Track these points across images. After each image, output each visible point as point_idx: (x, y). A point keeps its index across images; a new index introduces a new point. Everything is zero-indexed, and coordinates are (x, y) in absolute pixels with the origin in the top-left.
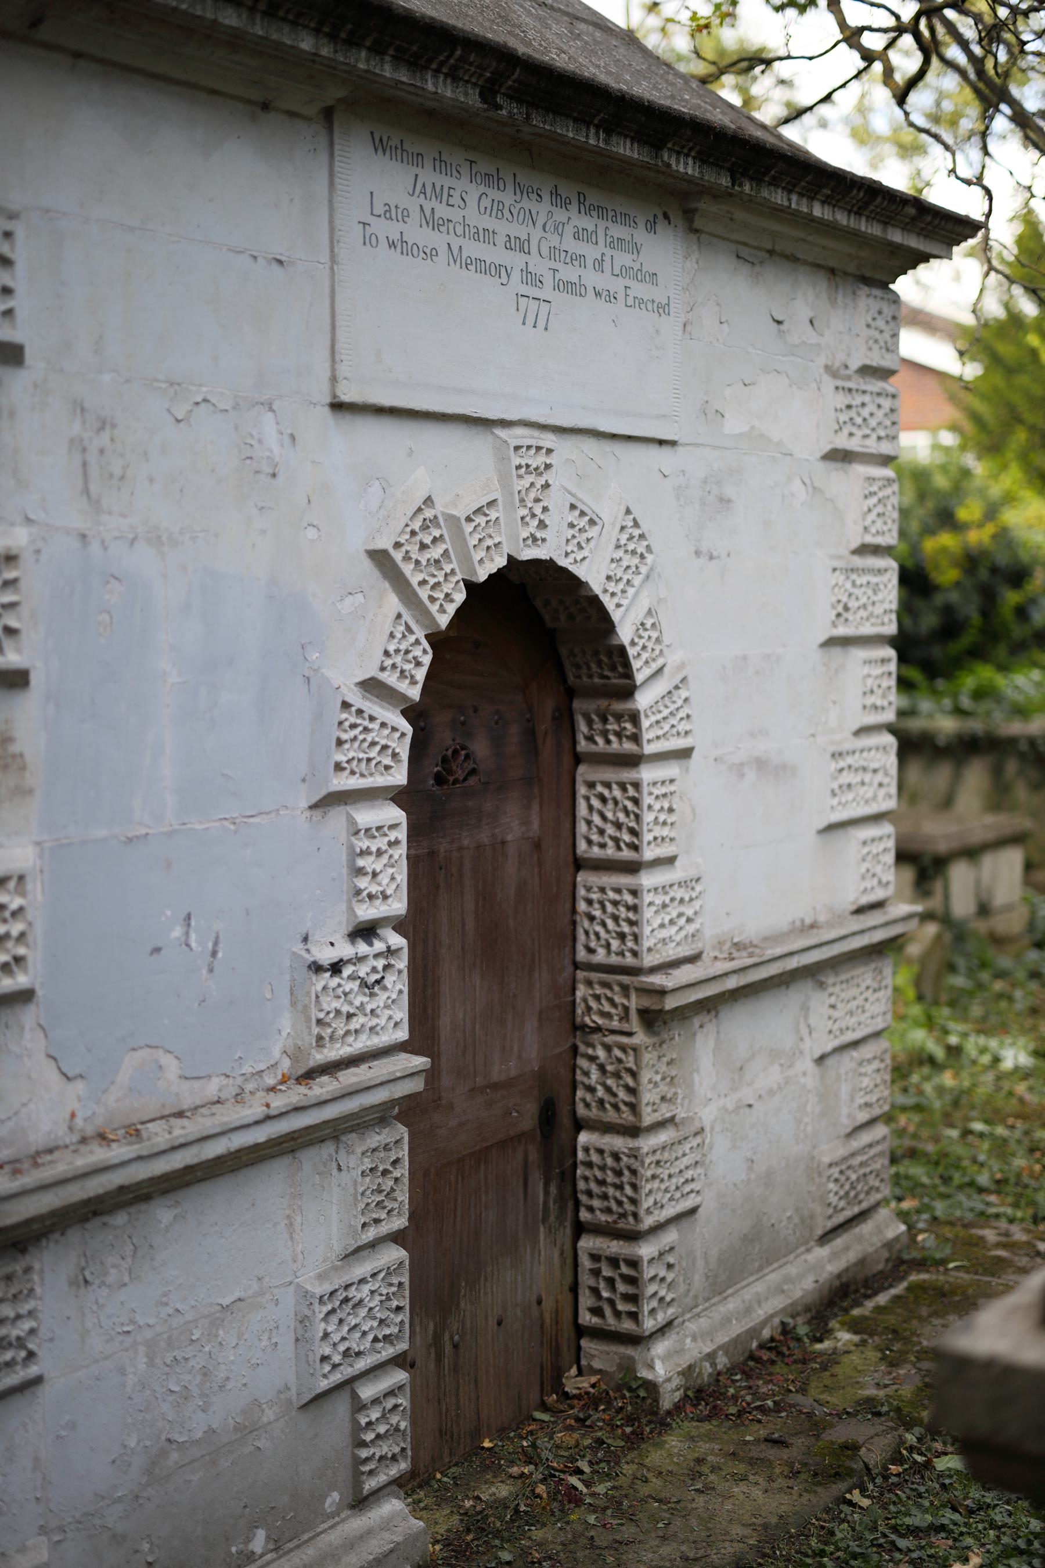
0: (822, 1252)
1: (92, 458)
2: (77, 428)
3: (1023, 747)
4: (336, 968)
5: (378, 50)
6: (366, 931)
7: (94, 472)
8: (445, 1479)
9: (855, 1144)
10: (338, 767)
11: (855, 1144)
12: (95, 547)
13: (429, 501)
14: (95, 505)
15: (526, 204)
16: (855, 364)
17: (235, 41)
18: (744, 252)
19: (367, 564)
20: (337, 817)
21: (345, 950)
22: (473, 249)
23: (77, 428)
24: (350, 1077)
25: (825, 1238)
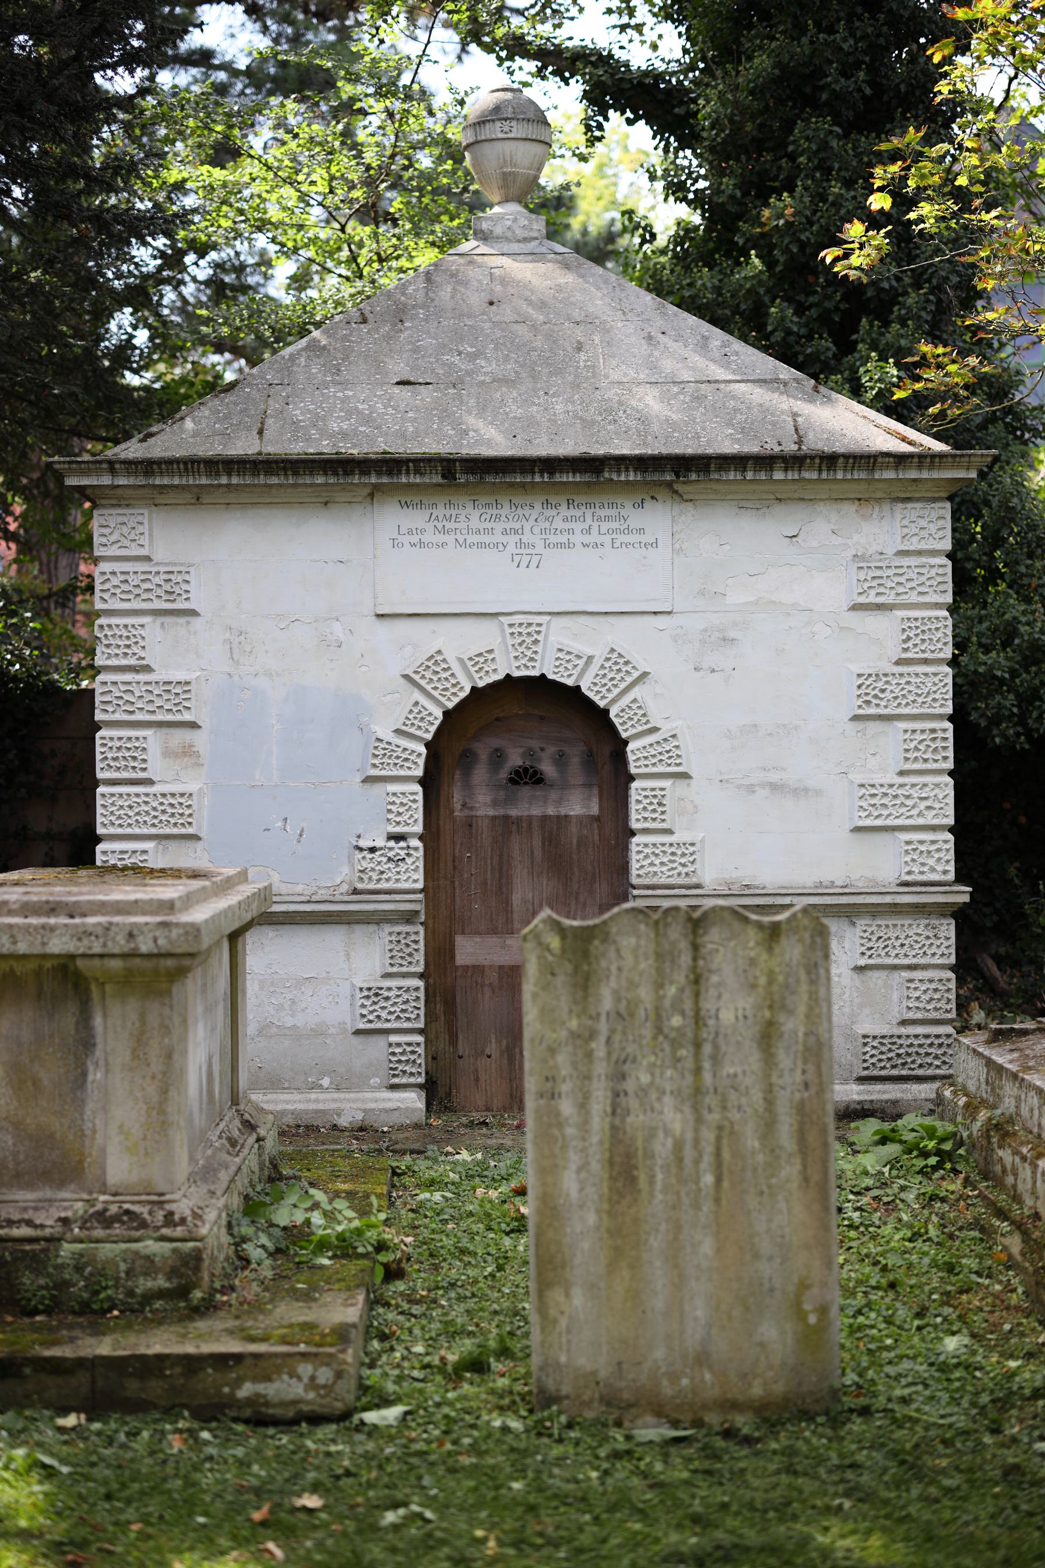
0: (855, 1087)
1: (235, 646)
2: (227, 635)
3: (493, 977)
4: (372, 850)
5: (311, 474)
6: (398, 838)
7: (236, 651)
8: (565, 1071)
9: (904, 1031)
10: (374, 766)
11: (904, 1031)
12: (236, 678)
13: (439, 652)
14: (237, 663)
15: (520, 511)
16: (890, 551)
17: (280, 485)
18: (744, 504)
19: (402, 681)
20: (379, 789)
21: (380, 842)
22: (486, 539)
23: (227, 635)
24: (398, 897)
25: (861, 1080)
